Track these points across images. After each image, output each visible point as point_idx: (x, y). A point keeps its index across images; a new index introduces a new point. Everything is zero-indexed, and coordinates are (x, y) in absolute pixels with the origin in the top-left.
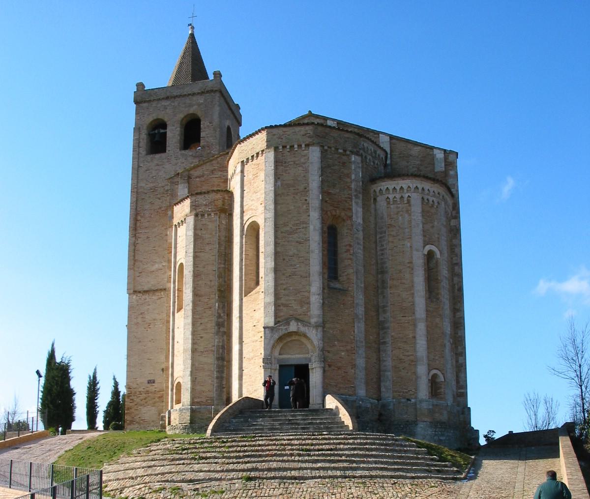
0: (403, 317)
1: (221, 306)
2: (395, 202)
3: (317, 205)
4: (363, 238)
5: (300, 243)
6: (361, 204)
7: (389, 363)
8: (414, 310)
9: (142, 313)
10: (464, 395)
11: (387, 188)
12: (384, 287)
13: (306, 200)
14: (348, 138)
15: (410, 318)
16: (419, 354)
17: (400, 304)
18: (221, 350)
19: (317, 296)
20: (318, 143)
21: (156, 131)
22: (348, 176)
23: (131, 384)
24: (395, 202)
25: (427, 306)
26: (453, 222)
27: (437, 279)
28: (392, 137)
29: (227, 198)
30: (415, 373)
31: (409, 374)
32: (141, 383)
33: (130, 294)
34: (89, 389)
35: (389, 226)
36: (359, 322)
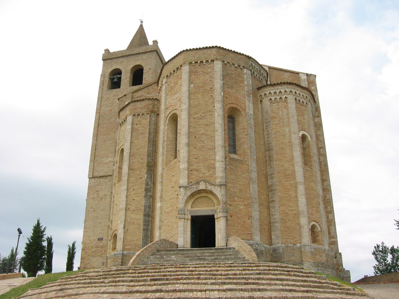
0: (286, 181)
1: (149, 177)
3: (220, 99)
4: (254, 125)
5: (207, 125)
6: (251, 101)
7: (277, 216)
9: (97, 191)
11: (270, 92)
12: (271, 161)
13: (212, 96)
14: (241, 58)
15: (292, 182)
16: (300, 209)
17: (284, 172)
18: (147, 210)
19: (220, 163)
21: (115, 77)
22: (242, 82)
26: (317, 120)
27: (310, 155)
30: (298, 224)
31: (294, 224)
32: (93, 240)
33: (90, 178)
34: (69, 253)
35: (272, 118)
36: (253, 184)
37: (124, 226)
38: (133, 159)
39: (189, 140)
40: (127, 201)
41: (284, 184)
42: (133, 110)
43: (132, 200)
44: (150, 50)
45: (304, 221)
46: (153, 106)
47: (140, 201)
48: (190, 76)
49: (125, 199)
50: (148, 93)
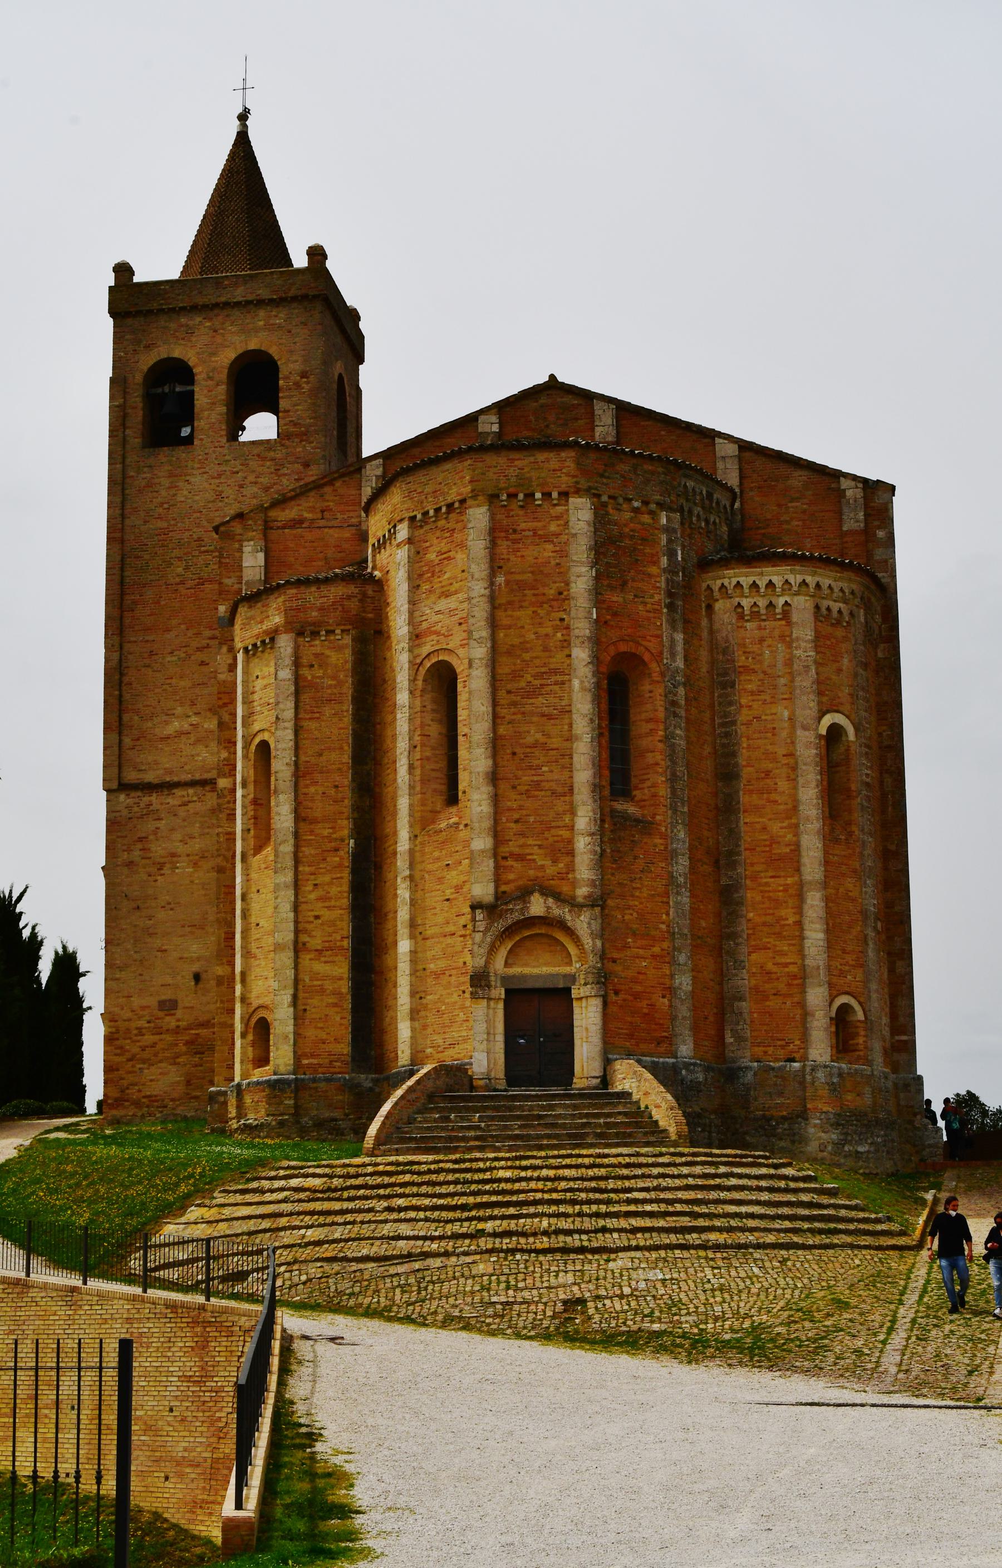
2: (755, 615)
5: (550, 717)
8: (798, 862)
9: (141, 839)
10: (908, 1048)
13: (562, 620)
15: (789, 881)
19: (588, 839)
20: (588, 490)
21: (166, 389)
23: (116, 1010)
24: (755, 615)
25: (826, 853)
28: (747, 448)
29: (370, 593)
30: (802, 1004)
36: (678, 893)
37: (295, 997)
38: (307, 786)
39: (495, 764)
40: (296, 922)
41: (767, 884)
42: (293, 613)
43: (312, 919)
44: (299, 293)
45: (816, 996)
46: (360, 601)
47: (336, 919)
48: (493, 544)
49: (292, 915)
50: (323, 511)
